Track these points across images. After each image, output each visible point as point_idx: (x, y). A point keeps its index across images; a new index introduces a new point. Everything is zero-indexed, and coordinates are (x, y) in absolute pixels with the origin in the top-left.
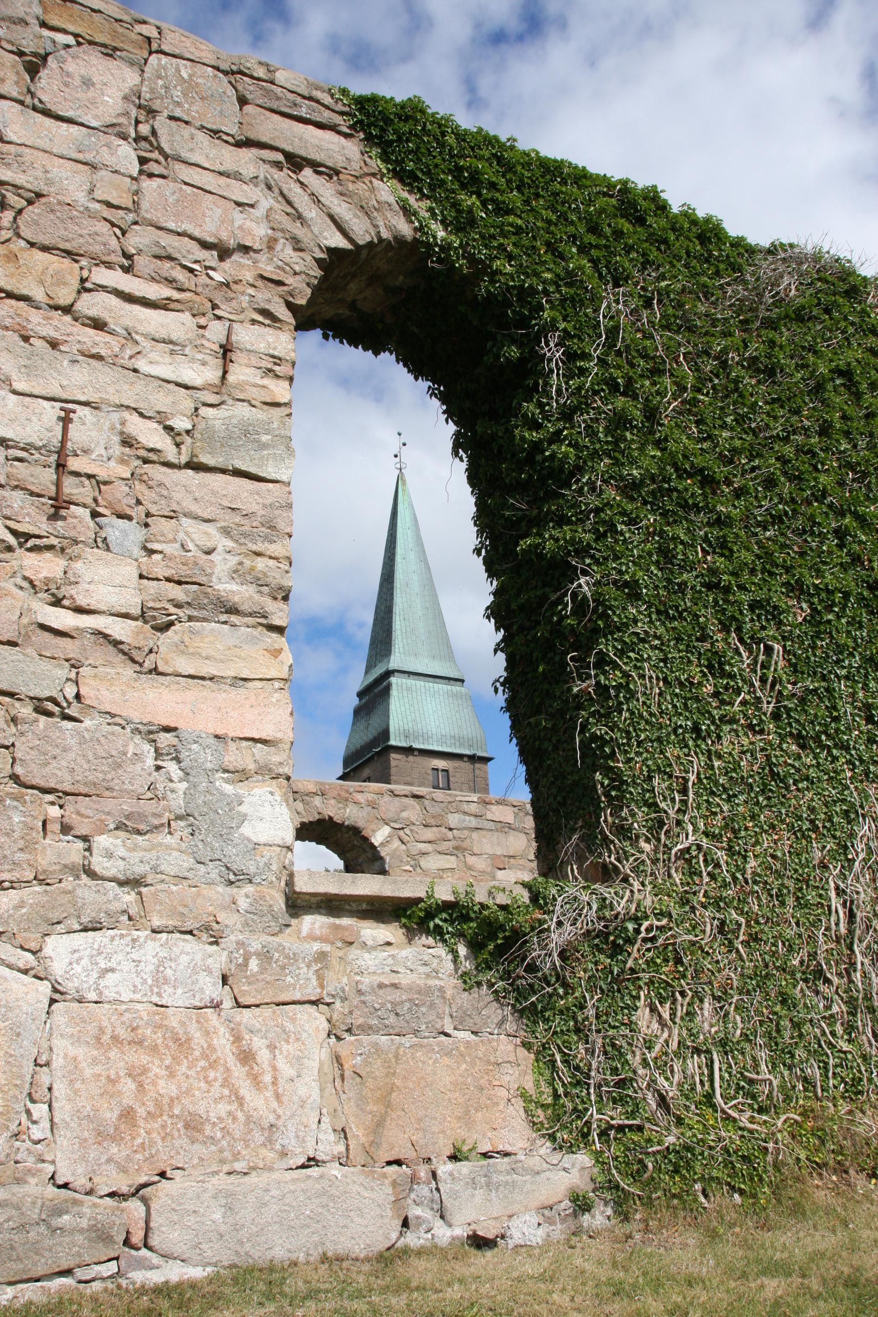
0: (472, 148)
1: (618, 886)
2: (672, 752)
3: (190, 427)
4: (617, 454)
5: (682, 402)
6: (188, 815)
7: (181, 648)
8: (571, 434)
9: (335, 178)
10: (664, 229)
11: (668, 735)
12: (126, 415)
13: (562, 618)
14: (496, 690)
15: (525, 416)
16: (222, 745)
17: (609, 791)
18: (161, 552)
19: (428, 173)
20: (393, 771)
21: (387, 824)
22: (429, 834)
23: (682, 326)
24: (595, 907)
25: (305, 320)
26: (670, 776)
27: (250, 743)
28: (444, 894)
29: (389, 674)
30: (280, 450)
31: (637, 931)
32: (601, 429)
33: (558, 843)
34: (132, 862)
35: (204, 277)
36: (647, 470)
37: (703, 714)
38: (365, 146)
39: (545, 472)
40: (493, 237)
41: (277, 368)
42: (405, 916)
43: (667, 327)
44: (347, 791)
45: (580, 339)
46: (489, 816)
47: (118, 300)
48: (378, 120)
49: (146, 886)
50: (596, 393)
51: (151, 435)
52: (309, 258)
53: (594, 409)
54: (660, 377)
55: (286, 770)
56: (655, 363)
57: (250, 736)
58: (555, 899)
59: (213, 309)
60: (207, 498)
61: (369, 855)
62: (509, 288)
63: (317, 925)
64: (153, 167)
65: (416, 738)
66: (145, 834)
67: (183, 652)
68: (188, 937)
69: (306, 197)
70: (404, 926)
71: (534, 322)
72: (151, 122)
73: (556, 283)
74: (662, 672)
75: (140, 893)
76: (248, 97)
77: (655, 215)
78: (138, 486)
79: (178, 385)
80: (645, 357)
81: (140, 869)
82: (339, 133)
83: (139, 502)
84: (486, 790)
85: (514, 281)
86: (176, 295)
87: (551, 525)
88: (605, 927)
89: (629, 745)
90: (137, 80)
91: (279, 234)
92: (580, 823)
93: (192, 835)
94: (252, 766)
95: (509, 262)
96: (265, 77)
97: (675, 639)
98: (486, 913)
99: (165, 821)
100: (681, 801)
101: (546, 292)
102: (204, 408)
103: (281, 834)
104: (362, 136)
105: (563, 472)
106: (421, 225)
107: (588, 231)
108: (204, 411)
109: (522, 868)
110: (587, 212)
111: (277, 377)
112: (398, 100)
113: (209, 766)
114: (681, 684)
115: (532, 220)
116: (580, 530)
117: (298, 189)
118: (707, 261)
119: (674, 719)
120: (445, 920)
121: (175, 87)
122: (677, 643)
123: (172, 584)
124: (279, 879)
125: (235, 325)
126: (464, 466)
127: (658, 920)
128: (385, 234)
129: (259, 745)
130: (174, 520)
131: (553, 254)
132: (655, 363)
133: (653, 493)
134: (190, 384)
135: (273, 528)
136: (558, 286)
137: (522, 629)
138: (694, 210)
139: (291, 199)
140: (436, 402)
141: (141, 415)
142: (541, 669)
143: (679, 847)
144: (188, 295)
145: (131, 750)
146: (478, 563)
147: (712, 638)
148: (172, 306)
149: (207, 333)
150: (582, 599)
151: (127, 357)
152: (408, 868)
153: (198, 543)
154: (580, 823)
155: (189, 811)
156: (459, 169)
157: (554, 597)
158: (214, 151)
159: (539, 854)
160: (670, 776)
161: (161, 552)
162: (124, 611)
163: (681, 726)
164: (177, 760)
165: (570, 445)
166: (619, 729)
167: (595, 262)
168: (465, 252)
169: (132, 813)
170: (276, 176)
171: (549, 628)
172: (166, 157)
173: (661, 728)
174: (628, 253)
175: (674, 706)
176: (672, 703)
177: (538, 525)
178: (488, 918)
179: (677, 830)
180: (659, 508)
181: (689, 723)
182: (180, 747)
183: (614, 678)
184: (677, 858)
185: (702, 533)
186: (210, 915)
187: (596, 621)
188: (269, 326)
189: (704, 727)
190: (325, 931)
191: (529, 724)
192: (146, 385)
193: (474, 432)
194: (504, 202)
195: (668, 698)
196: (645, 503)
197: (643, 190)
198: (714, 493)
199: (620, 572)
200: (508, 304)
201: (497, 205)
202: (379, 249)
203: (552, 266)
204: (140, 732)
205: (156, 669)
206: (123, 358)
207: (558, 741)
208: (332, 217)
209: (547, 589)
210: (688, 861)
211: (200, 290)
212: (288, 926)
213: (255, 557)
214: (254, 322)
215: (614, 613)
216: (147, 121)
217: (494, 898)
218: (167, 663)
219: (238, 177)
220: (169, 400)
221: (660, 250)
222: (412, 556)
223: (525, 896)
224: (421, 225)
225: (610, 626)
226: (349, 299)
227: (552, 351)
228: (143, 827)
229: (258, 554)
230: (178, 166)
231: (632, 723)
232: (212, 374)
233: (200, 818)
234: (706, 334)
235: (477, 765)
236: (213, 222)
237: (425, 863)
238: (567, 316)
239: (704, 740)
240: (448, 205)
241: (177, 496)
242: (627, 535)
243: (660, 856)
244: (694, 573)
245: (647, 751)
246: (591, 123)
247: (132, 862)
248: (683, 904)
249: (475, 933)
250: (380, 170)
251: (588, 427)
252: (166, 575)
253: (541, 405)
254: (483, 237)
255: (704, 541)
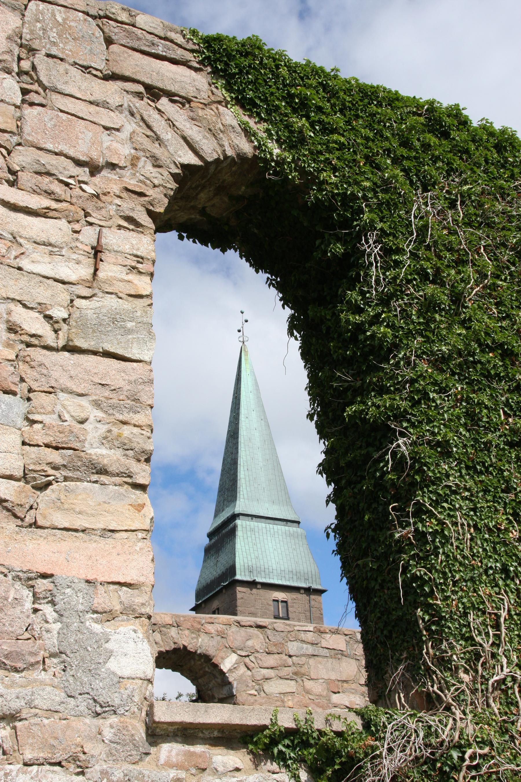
0: (302, 78)
1: (441, 715)
2: (484, 590)
3: (66, 316)
4: (428, 333)
5: (483, 287)
6: (61, 653)
7: (58, 505)
8: (388, 317)
9: (187, 106)
10: (466, 141)
11: (480, 575)
12: (12, 306)
13: (384, 474)
14: (328, 536)
15: (349, 302)
16: (92, 589)
17: (430, 626)
18: (41, 422)
19: (265, 101)
20: (239, 602)
21: (234, 652)
22: (271, 660)
23: (482, 223)
24: (421, 734)
25: (163, 223)
26: (484, 613)
27: (116, 587)
28: (286, 722)
29: (234, 517)
30: (143, 335)
31: (462, 759)
32: (414, 312)
33: (386, 673)
34: (9, 698)
35: (78, 190)
36: (454, 346)
37: (511, 557)
38: (212, 78)
39: (366, 349)
40: (320, 153)
41: (139, 266)
42: (252, 743)
43: (469, 224)
44: (199, 623)
45: (394, 236)
46: (324, 644)
47: (4, 209)
48: (223, 56)
49: (20, 720)
50: (409, 282)
51: (33, 323)
52: (166, 173)
53: (407, 295)
54: (463, 266)
55: (147, 610)
56: (459, 255)
57: (116, 580)
58: (385, 727)
59: (86, 217)
60: (81, 376)
61: (219, 681)
62: (334, 195)
63: (174, 753)
64: (33, 97)
65: (259, 572)
66: (22, 671)
67: (59, 508)
68: (57, 768)
69: (163, 122)
70: (251, 752)
71: (355, 223)
72: (31, 58)
73: (374, 190)
74: (472, 519)
75: (14, 728)
76: (114, 37)
77: (458, 130)
78: (22, 366)
79: (56, 280)
80: (450, 250)
81: (16, 705)
82: (190, 67)
83: (22, 380)
84: (320, 619)
85: (338, 189)
86: (54, 205)
87: (373, 394)
88: (432, 753)
89: (445, 585)
90: (19, 23)
91: (141, 154)
92: (405, 655)
93: (64, 671)
94: (118, 607)
95: (334, 173)
96: (127, 21)
97: (483, 490)
98: (324, 739)
99: (40, 658)
100: (494, 635)
101: (365, 198)
102: (78, 300)
103: (142, 667)
104: (209, 69)
105: (383, 349)
106: (260, 144)
107: (400, 145)
108: (78, 302)
109: (354, 692)
110: (399, 129)
111: (140, 273)
112: (239, 39)
113: (81, 607)
114: (490, 530)
115: (353, 137)
116: (397, 398)
117: (156, 115)
118: (503, 166)
119: (485, 561)
120: (288, 747)
121: (51, 29)
122: (485, 494)
123: (51, 449)
124: (140, 709)
125: (104, 230)
126: (298, 344)
127: (481, 748)
128: (230, 152)
129: (124, 588)
130: (53, 395)
131: (371, 166)
132: (459, 255)
133: (460, 365)
134: (66, 280)
135: (136, 400)
136: (375, 192)
137: (349, 483)
138: (491, 123)
139: (151, 124)
140: (273, 291)
141: (25, 306)
142: (367, 517)
143: (496, 678)
144: (64, 205)
145: (12, 595)
146: (311, 426)
147: (515, 489)
148: (51, 214)
149: (80, 237)
150: (401, 457)
151: (12, 257)
152: (253, 692)
153: (73, 414)
154: (405, 655)
155: (62, 649)
156: (291, 96)
157: (376, 456)
158: (86, 84)
159: (369, 683)
160: (484, 613)
161: (41, 422)
162: (8, 473)
163: (491, 568)
164: (53, 603)
165: (388, 326)
166: (437, 571)
167: (406, 171)
168: (296, 165)
169: (11, 652)
170: (137, 105)
171: (373, 482)
172: (45, 88)
173: (474, 569)
174: (435, 162)
175: (485, 550)
176: (482, 547)
177: (362, 395)
178: (326, 744)
179: (492, 662)
180: (466, 378)
181: (498, 565)
182: (55, 591)
183: (430, 526)
184: (494, 689)
185: (503, 399)
186: (77, 746)
187: (413, 476)
188: (133, 230)
189: (512, 569)
190: (181, 758)
191: (358, 565)
192: (29, 281)
193: (306, 316)
194: (329, 123)
195: (479, 542)
196: (453, 374)
197: (447, 108)
198: (513, 364)
199: (433, 434)
200: (333, 208)
201: (323, 125)
202: (225, 164)
203: (370, 176)
204: (20, 579)
205: (35, 523)
206: (9, 258)
207: (384, 581)
208: (185, 139)
209: (370, 449)
210: (505, 692)
211: (74, 200)
212: (147, 754)
213: (121, 425)
214: (120, 227)
215: (429, 469)
216: (28, 58)
217: (330, 725)
218: (45, 518)
219: (106, 106)
220: (49, 293)
221: (463, 159)
222: (254, 415)
223: (358, 724)
224: (260, 144)
225: (425, 480)
226: (200, 206)
227: (371, 247)
228: (20, 665)
229: (124, 423)
230: (55, 97)
231: (448, 565)
232: (85, 271)
233: (72, 655)
234: (503, 228)
235: (312, 597)
236: (85, 143)
237: (269, 687)
238: (383, 217)
239: (513, 580)
240: (282, 127)
241: (55, 374)
242: (438, 402)
243: (479, 686)
244: (498, 433)
245: (462, 590)
246: (400, 58)
247: (9, 698)
248: (503, 733)
249: (315, 758)
250: (225, 98)
251: (403, 310)
252: (46, 442)
253: (362, 293)
254: (311, 153)
255: (506, 406)
